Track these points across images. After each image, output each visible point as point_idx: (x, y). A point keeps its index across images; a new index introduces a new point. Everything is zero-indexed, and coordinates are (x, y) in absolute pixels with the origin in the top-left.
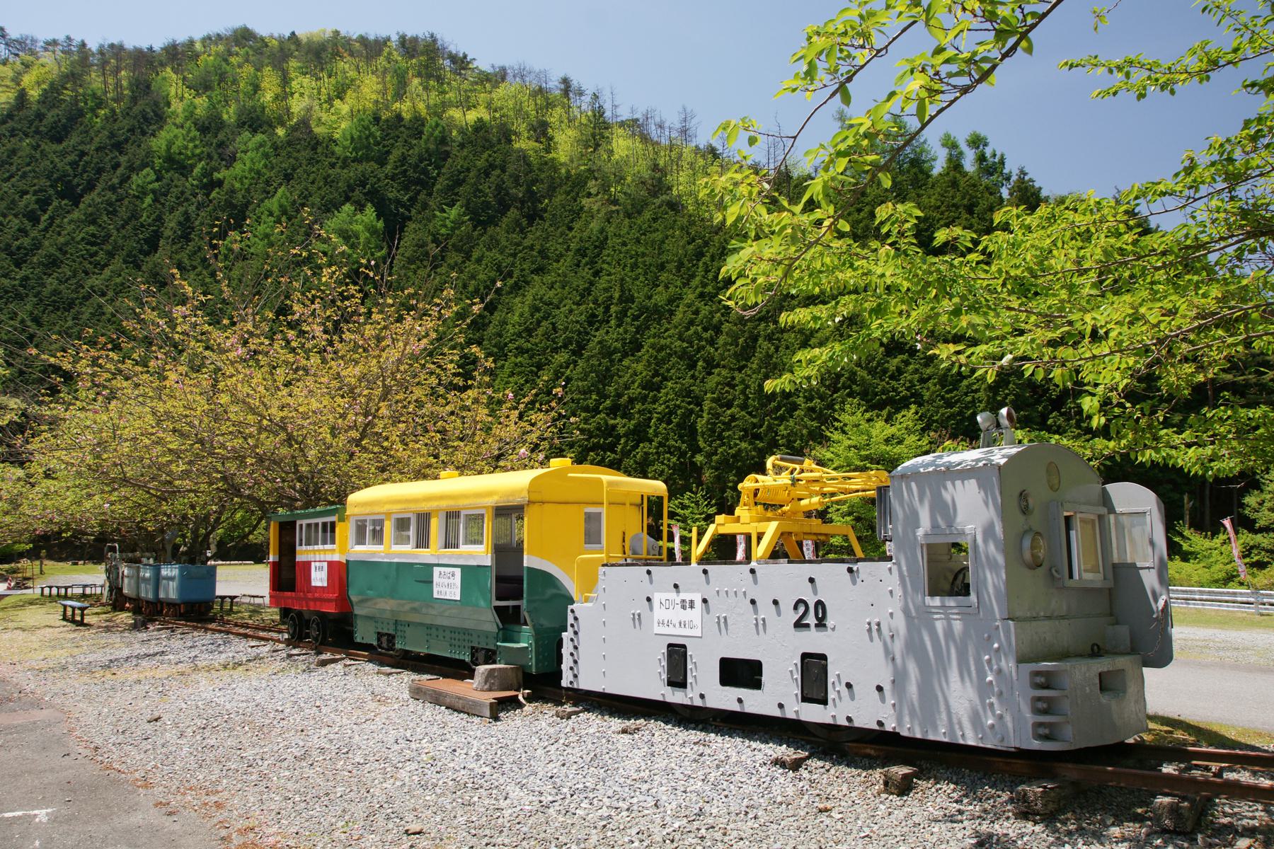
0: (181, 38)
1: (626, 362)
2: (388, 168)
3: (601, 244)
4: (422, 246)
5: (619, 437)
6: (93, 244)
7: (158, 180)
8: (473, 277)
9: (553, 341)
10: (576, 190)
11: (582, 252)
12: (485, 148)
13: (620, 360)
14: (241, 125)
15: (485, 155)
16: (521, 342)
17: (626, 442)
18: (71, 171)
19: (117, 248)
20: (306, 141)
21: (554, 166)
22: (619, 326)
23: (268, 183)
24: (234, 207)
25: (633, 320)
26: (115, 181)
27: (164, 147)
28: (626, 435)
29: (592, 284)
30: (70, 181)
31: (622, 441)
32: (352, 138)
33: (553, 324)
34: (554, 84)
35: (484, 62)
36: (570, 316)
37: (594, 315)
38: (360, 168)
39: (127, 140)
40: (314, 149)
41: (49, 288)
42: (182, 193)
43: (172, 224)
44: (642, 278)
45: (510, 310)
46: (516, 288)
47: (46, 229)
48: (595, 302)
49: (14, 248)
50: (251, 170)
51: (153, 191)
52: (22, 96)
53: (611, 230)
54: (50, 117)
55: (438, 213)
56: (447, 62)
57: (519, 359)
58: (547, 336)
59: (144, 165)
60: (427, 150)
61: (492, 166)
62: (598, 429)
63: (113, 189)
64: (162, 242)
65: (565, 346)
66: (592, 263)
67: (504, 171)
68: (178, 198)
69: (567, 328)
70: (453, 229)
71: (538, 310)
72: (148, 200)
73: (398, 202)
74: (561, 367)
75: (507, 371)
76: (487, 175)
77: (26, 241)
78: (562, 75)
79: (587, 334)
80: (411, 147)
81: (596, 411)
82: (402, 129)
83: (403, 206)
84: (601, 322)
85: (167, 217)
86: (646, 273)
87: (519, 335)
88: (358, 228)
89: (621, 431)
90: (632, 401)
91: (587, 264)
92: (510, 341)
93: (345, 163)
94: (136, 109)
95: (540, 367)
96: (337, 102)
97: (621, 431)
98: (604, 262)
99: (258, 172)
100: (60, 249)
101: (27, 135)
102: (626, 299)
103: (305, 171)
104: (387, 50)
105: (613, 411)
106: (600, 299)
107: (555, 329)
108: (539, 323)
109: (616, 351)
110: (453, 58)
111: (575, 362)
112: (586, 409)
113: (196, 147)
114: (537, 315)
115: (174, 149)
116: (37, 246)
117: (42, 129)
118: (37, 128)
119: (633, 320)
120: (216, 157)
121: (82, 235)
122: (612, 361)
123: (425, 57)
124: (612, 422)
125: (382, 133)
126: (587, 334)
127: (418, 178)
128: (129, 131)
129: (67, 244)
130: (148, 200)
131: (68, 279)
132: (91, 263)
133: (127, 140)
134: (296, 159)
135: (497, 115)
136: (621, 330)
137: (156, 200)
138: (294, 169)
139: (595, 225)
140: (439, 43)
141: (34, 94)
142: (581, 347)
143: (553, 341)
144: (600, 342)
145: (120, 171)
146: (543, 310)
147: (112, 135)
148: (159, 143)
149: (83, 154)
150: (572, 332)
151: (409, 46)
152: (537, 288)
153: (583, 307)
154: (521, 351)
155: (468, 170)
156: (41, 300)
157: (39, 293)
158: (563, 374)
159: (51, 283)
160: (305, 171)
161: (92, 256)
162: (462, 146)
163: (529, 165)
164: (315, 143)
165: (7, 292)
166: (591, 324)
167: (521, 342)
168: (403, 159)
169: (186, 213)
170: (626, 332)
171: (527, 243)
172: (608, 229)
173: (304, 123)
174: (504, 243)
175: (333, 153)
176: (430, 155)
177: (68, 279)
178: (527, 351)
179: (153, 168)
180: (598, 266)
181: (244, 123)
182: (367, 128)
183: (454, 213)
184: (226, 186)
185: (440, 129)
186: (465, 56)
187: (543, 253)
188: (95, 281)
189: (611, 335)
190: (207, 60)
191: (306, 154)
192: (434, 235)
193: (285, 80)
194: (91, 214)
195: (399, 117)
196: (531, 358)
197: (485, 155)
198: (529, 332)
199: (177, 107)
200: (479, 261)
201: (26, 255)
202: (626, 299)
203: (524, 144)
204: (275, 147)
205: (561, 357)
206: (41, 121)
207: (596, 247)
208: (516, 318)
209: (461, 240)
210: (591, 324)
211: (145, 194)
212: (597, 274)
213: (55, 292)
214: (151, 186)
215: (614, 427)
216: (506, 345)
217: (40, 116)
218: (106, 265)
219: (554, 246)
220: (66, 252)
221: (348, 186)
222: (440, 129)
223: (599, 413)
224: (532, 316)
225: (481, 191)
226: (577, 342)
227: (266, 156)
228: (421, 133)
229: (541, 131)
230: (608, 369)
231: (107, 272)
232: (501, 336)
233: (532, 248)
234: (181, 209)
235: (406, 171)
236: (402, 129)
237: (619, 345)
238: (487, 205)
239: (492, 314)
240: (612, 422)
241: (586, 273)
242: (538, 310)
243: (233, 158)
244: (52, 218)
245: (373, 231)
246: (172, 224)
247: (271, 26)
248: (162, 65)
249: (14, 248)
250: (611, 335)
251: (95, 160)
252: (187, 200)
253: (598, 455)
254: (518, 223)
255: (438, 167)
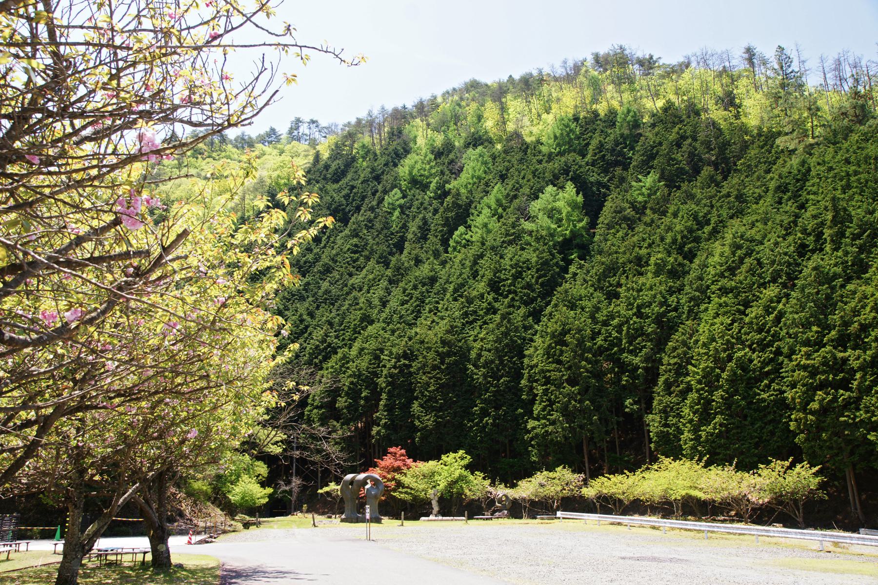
0: (426, 97)
1: (850, 287)
2: (589, 158)
3: (804, 175)
4: (620, 212)
5: (853, 372)
6: (355, 252)
7: (404, 197)
8: (669, 229)
9: (760, 276)
10: (770, 142)
11: (782, 189)
12: (674, 124)
13: (843, 286)
14: (467, 145)
15: (676, 129)
16: (723, 282)
17: (863, 377)
18: (344, 202)
19: (372, 252)
20: (520, 149)
21: (744, 129)
22: (836, 249)
23: (487, 185)
24: (460, 206)
25: (853, 239)
26: (374, 203)
27: (407, 172)
28: (862, 368)
29: (797, 216)
30: (344, 209)
31: (858, 376)
32: (556, 137)
33: (758, 260)
34: (738, 63)
35: (670, 58)
36: (775, 248)
37: (803, 246)
38: (563, 159)
39: (383, 173)
40: (525, 152)
41: (323, 289)
42: (422, 204)
43: (414, 229)
44: (857, 197)
45: (711, 254)
46: (715, 232)
47: (325, 247)
48: (804, 231)
49: (302, 262)
50: (473, 176)
51: (401, 206)
52: (317, 157)
53: (812, 161)
54: (334, 166)
55: (634, 183)
56: (636, 66)
57: (724, 299)
58: (751, 271)
59: (394, 187)
60: (622, 135)
61: (683, 138)
62: (825, 363)
63: (372, 209)
64: (407, 244)
65: (774, 280)
66: (796, 196)
67: (695, 139)
68: (418, 208)
69: (773, 262)
70: (649, 196)
71: (739, 247)
72: (397, 213)
73: (599, 184)
74: (771, 301)
75: (711, 312)
76: (679, 146)
77: (310, 257)
78: (746, 45)
79: (798, 265)
80: (607, 135)
81: (819, 344)
82: (599, 122)
83: (603, 187)
84: (813, 251)
85: (410, 225)
86: (862, 191)
87: (722, 275)
88: (560, 204)
89: (855, 364)
90: (864, 328)
91: (789, 199)
92: (713, 283)
93: (550, 157)
94: (391, 148)
95: (747, 304)
96: (544, 116)
97: (855, 364)
98: (808, 194)
99: (479, 178)
100: (333, 259)
101: (318, 182)
102: (841, 219)
103: (517, 170)
104: (584, 69)
105: (842, 342)
106: (809, 227)
107: (760, 263)
108: (741, 261)
109: (836, 276)
110: (641, 63)
111: (787, 296)
112: (807, 343)
113: (431, 168)
114: (739, 252)
115: (415, 172)
116: (317, 259)
117: (329, 176)
118: (325, 176)
119: (853, 239)
120: (447, 172)
121: (348, 246)
122: (833, 288)
123: (616, 64)
124: (840, 355)
125: (582, 130)
126: (798, 265)
127: (616, 161)
128: (385, 165)
129: (337, 255)
130: (397, 213)
131: (337, 281)
132: (354, 267)
133: (383, 173)
134: (509, 161)
135: (685, 98)
136: (840, 253)
137: (402, 212)
138: (508, 170)
139: (795, 161)
140: (626, 52)
141: (325, 155)
142: (792, 278)
143: (760, 276)
144: (815, 269)
145: (378, 194)
146: (744, 248)
147: (373, 170)
148: (403, 170)
149: (353, 187)
150: (780, 264)
151: (601, 62)
152: (735, 227)
153: (790, 239)
154: (724, 291)
155: (660, 144)
156: (317, 299)
157: (316, 293)
158: (774, 309)
159: (325, 285)
160: (517, 170)
161: (354, 261)
162: (653, 125)
163: (720, 130)
164: (525, 148)
165: (293, 295)
166: (801, 255)
167: (723, 282)
168: (601, 146)
169: (424, 218)
170: (846, 253)
171: (724, 191)
172: (809, 161)
173: (517, 135)
174: (699, 196)
175: (540, 152)
176: (625, 139)
177: (337, 281)
178: (731, 291)
179: (400, 189)
180: (803, 199)
181: (469, 144)
182: (567, 126)
183: (649, 180)
184: (453, 192)
185: (631, 114)
186: (651, 58)
187: (740, 198)
188: (355, 280)
189: (828, 260)
190: (446, 107)
191: (519, 156)
192: (631, 203)
193: (503, 109)
194: (355, 230)
195: (596, 114)
196: (736, 297)
197: (676, 129)
198: (732, 271)
199: (421, 141)
200: (675, 215)
201: (310, 267)
202: (841, 219)
203: (717, 114)
204: (494, 157)
205: (771, 291)
206: (327, 170)
207: (798, 181)
208: (717, 258)
209: (658, 203)
210: (801, 255)
211: (394, 209)
212: (802, 207)
213: (327, 292)
214: (398, 203)
215: (845, 360)
216: (708, 287)
217: (327, 167)
218: (364, 267)
219: (750, 191)
220: (336, 261)
221: (554, 176)
222: (631, 114)
223: (824, 346)
224: (734, 253)
225: (673, 159)
226: (788, 274)
227: (485, 163)
228: (614, 124)
229: (729, 101)
230: (828, 297)
231: (364, 271)
232: (701, 279)
233: (728, 195)
234: (421, 216)
235: (604, 156)
236: (599, 122)
237: (839, 270)
238: (681, 171)
239: (691, 262)
240: (840, 355)
241: (790, 207)
242: (739, 247)
243: (461, 170)
244: (329, 237)
245: (573, 205)
246: (414, 229)
247: (491, 78)
248: (413, 117)
249: (302, 262)
250: (828, 260)
251: (360, 191)
252: (425, 209)
253: (828, 394)
254: (712, 179)
255: (632, 148)
